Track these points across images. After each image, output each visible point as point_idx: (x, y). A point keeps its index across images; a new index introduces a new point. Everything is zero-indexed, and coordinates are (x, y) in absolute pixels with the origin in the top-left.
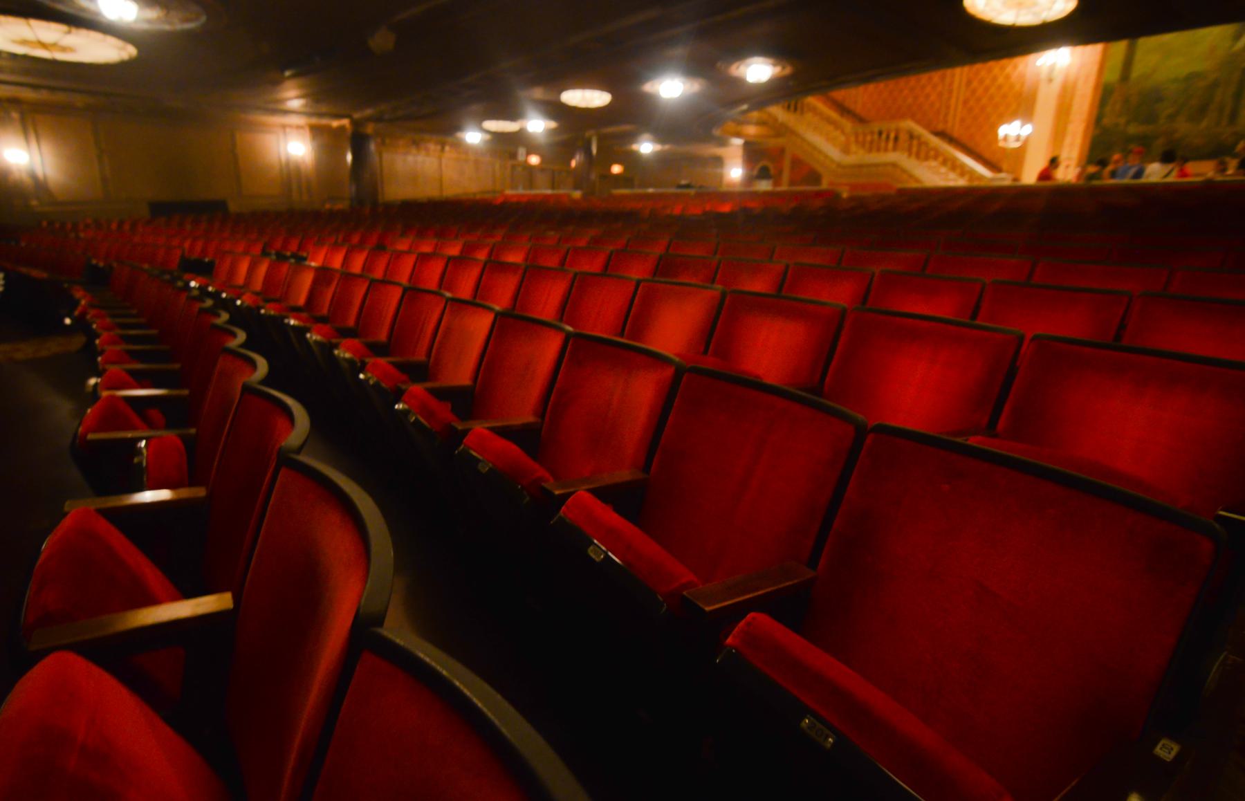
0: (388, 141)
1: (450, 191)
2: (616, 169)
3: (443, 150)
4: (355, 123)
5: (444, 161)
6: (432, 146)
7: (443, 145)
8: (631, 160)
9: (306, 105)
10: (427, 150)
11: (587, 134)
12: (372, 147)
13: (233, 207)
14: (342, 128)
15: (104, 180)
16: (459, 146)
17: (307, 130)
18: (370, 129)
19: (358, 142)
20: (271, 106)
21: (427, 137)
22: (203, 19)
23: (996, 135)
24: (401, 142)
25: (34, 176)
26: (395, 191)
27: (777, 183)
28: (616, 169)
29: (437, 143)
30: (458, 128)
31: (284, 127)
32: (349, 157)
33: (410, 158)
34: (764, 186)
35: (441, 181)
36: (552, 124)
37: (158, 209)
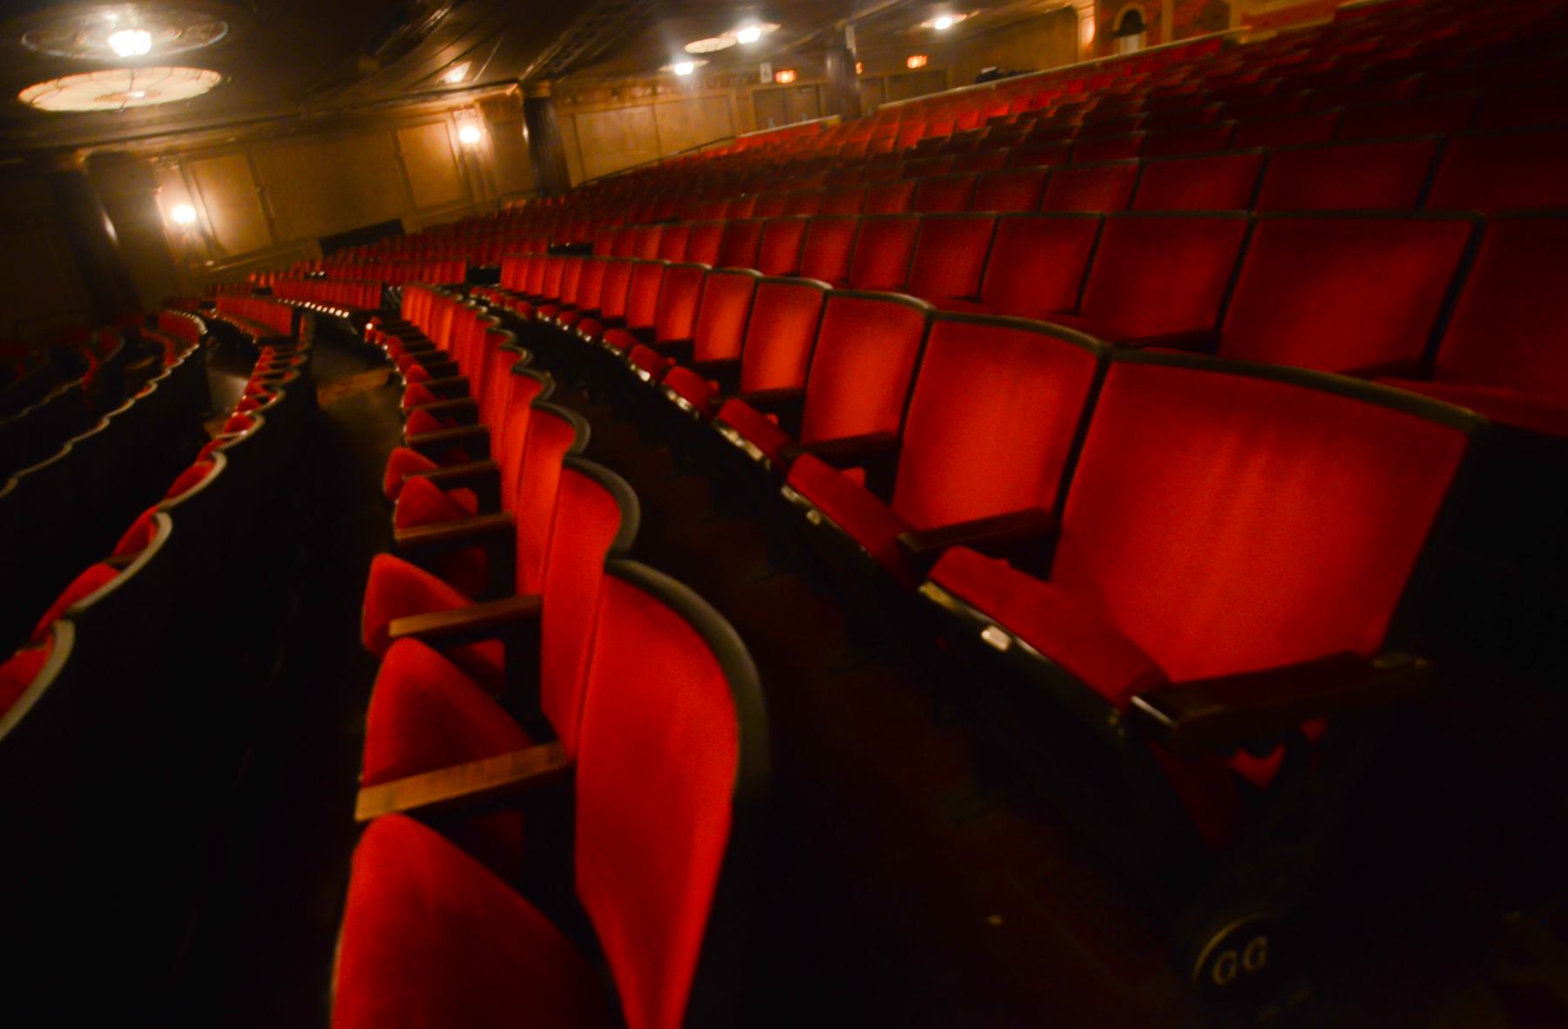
0: (580, 99)
1: (672, 151)
2: (915, 62)
3: (654, 93)
4: (527, 86)
5: (659, 109)
6: (638, 92)
7: (653, 85)
8: (924, 43)
9: (473, 71)
10: (633, 98)
11: (839, 24)
12: (551, 113)
13: (410, 227)
14: (513, 95)
15: (270, 222)
16: (671, 82)
17: (477, 111)
18: (544, 90)
19: (533, 110)
20: (191, 178)
21: (630, 80)
22: (226, 27)
23: (368, 563)
24: (598, 96)
25: (203, 233)
26: (604, 163)
27: (1153, 38)
28: (915, 62)
29: (646, 85)
30: (665, 59)
31: (451, 110)
32: (526, 133)
33: (613, 115)
34: (1133, 45)
35: (658, 139)
36: (772, 28)
37: (331, 245)
